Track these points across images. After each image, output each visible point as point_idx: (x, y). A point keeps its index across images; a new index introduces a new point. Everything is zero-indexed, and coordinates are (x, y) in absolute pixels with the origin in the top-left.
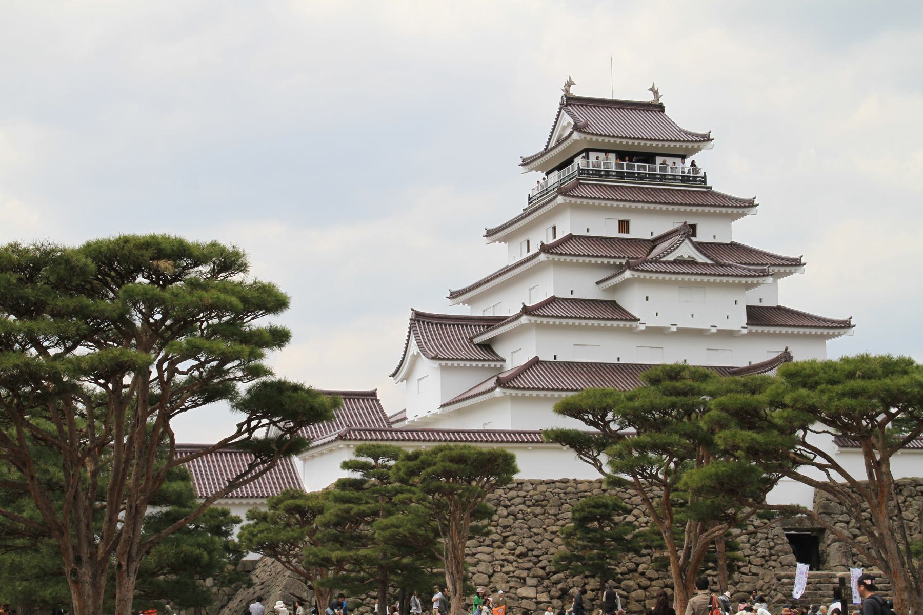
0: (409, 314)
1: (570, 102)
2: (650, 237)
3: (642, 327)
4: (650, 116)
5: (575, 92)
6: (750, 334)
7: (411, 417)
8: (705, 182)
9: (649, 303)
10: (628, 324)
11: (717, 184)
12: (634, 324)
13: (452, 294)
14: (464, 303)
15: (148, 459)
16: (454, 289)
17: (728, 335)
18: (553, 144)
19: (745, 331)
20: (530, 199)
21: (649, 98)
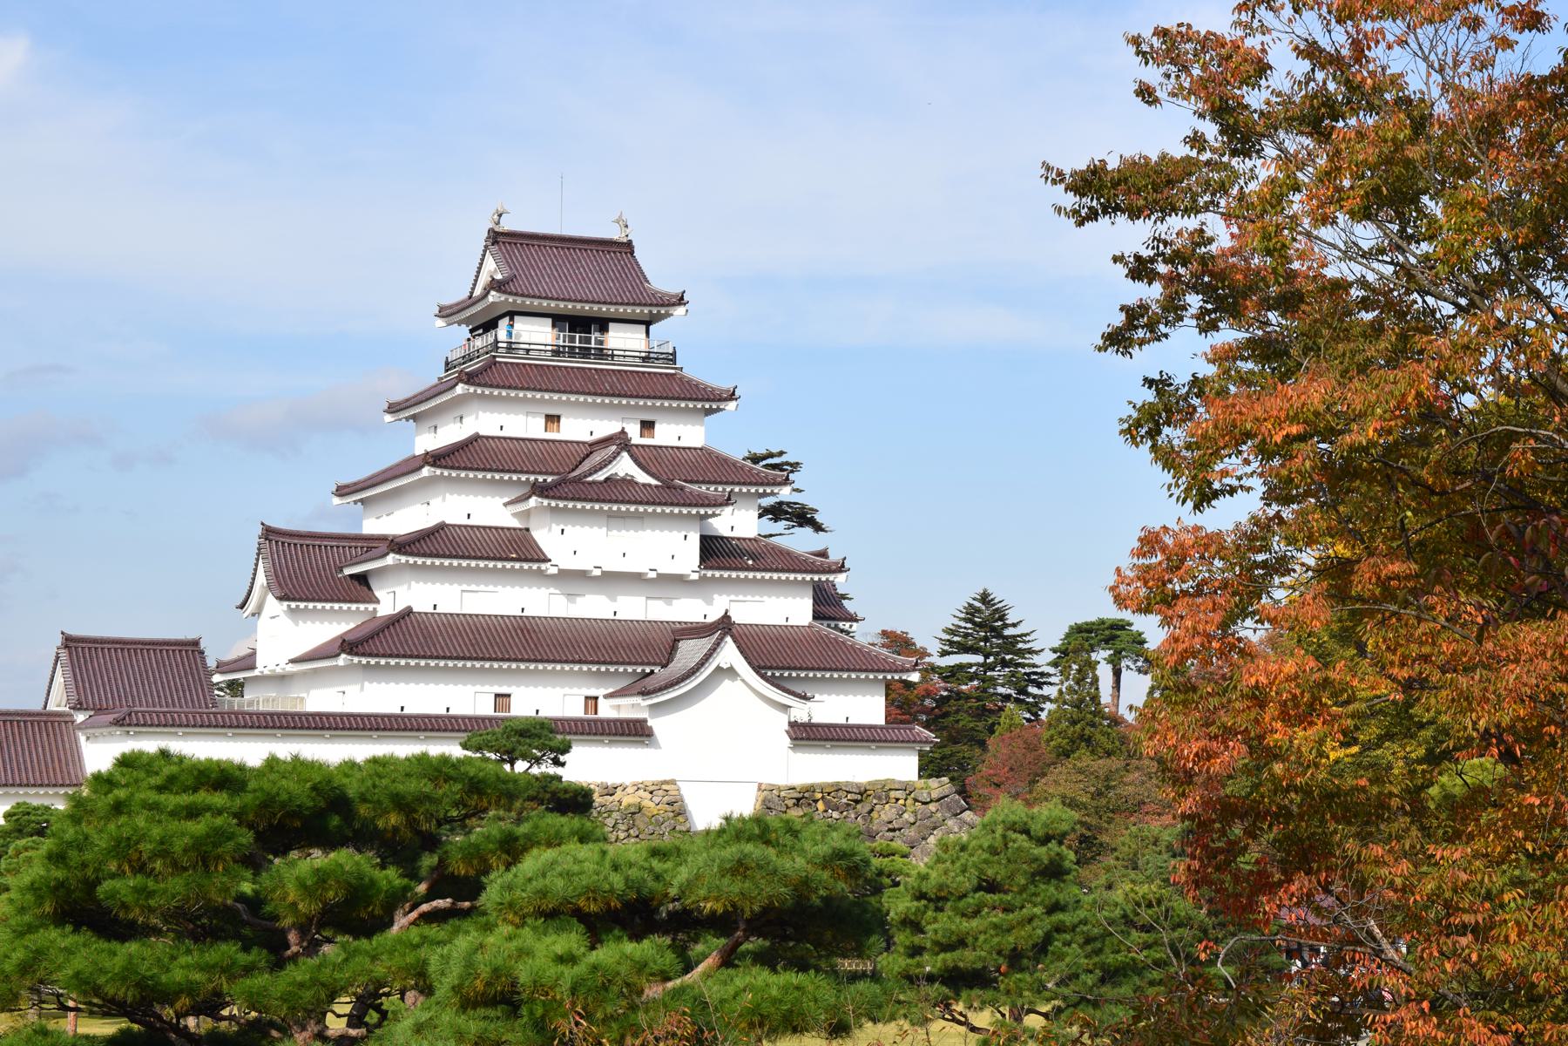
0: (259, 530)
1: (496, 238)
2: (588, 439)
3: (554, 571)
4: (608, 260)
5: (507, 225)
6: (703, 579)
7: (1113, 163)
8: (674, 361)
9: (572, 541)
10: (535, 566)
11: (693, 367)
12: (543, 566)
13: (441, 309)
14: (407, 419)
15: (1242, 652)
16: (447, 302)
17: (671, 583)
18: (478, 292)
19: (695, 576)
20: (447, 363)
21: (615, 234)
